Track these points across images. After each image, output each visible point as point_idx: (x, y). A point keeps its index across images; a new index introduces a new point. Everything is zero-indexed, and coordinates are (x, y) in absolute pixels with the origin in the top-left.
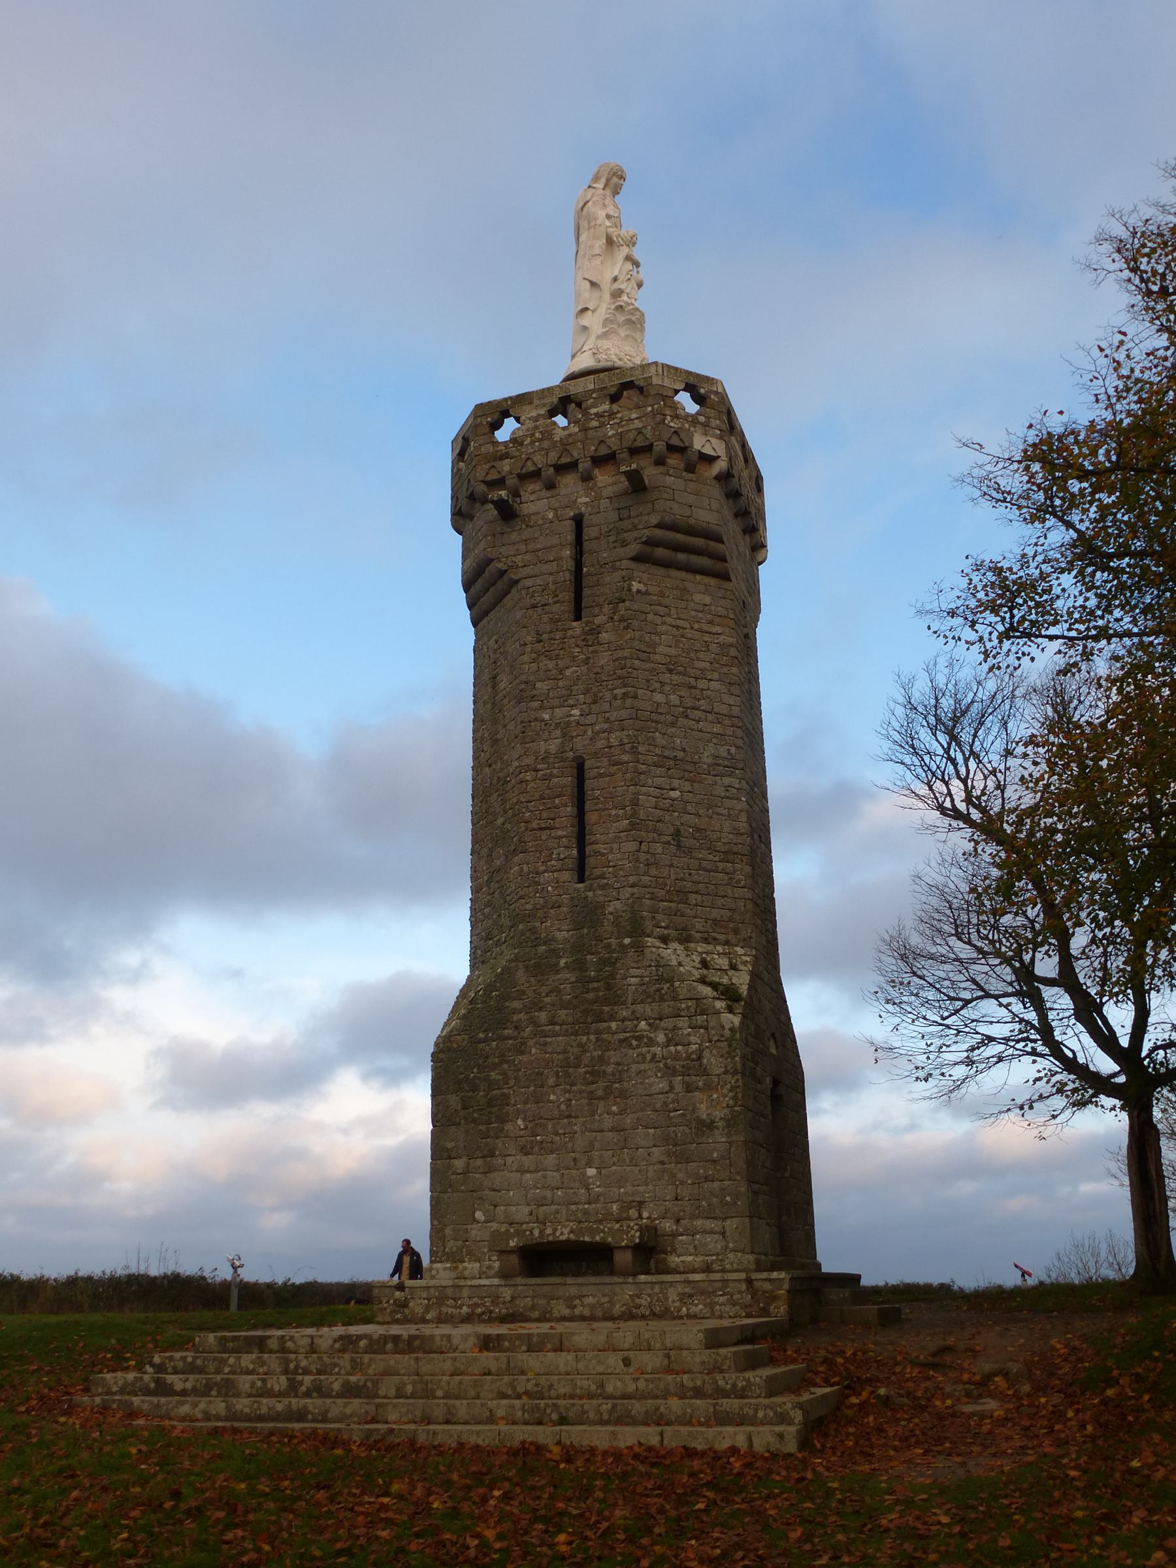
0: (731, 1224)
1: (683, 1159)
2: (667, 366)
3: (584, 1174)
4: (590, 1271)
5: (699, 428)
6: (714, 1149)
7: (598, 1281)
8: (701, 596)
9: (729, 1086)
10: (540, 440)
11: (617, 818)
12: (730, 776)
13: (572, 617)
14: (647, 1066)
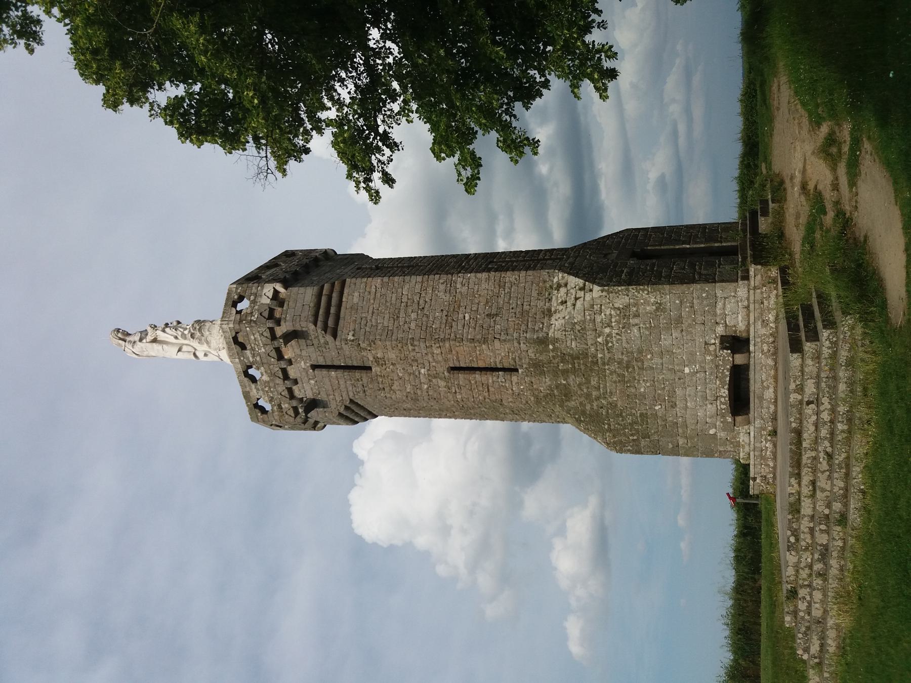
0: (719, 293)
1: (679, 320)
2: (223, 317)
3: (688, 374)
4: (747, 373)
5: (259, 299)
6: (674, 302)
7: (753, 373)
8: (355, 298)
9: (636, 293)
10: (270, 388)
11: (481, 351)
12: (456, 283)
13: (369, 371)
14: (624, 338)
